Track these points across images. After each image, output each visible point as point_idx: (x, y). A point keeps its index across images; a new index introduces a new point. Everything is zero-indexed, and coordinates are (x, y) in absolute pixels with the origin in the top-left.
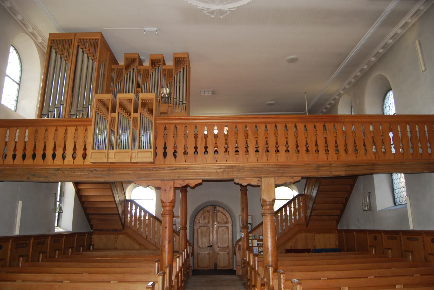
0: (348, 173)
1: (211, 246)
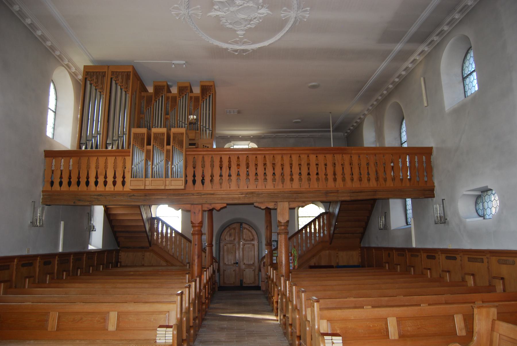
0: (353, 198)
1: (237, 263)
